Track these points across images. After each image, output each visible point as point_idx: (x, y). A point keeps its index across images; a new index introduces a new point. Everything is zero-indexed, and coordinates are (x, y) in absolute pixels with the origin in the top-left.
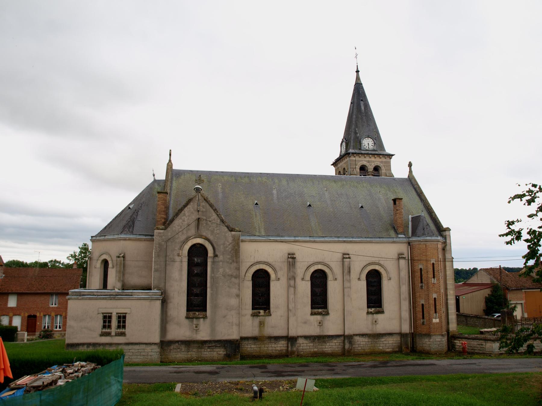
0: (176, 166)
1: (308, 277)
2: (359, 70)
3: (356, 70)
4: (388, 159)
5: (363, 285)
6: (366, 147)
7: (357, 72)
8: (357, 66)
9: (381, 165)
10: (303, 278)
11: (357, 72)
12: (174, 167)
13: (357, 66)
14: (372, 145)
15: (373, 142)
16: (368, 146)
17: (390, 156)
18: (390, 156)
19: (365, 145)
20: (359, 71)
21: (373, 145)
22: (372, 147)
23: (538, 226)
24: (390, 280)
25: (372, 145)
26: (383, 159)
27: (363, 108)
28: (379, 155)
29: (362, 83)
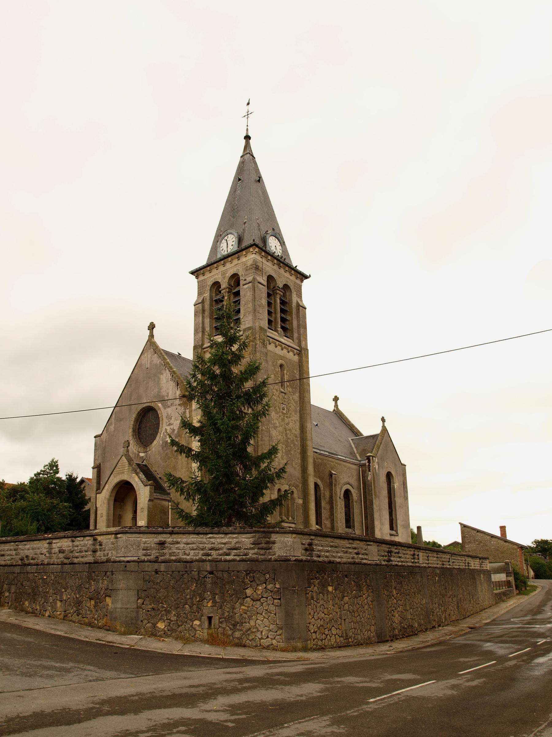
7: (247, 138)
11: (247, 138)
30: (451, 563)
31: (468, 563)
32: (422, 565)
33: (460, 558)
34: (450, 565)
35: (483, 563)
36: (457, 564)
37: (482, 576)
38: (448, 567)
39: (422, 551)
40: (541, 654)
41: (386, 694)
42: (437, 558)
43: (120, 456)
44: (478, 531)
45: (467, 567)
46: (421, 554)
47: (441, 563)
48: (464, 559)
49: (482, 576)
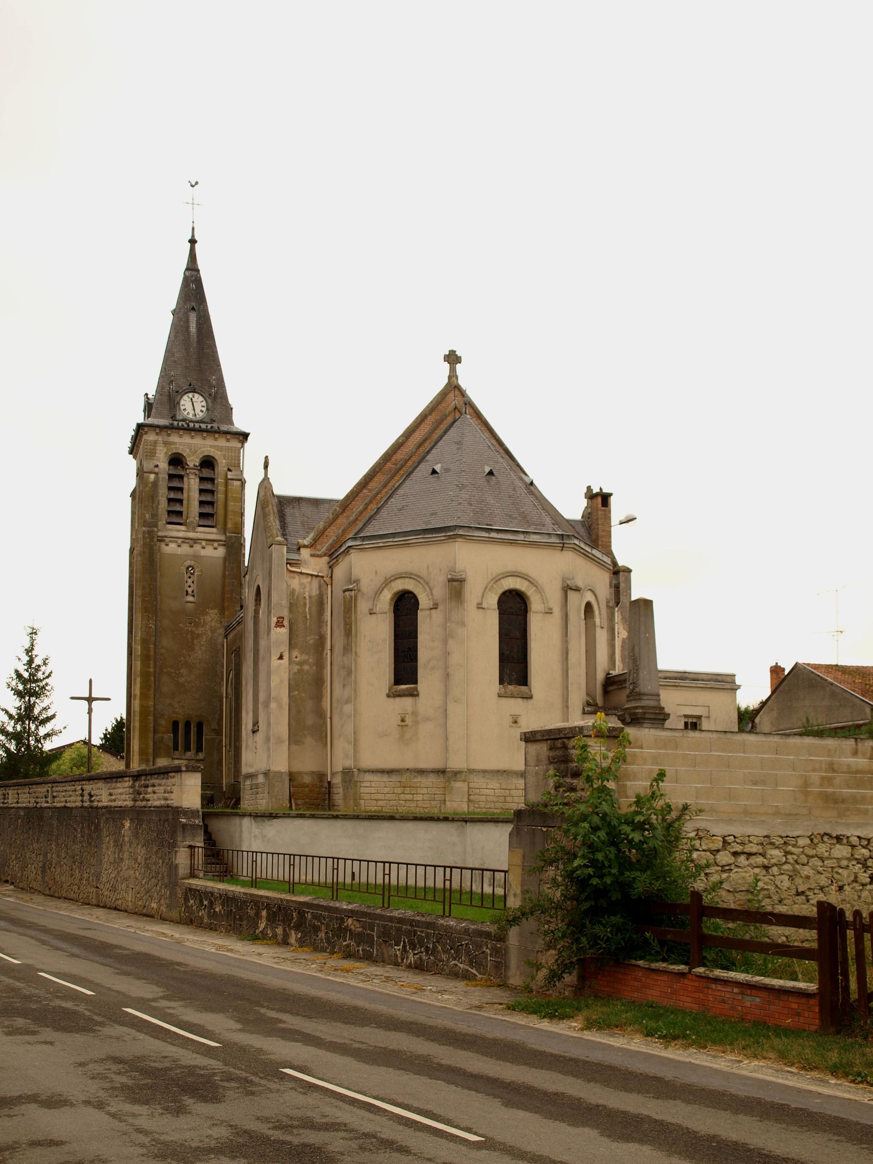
0: (280, 489)
1: (492, 600)
2: (196, 238)
3: (190, 238)
4: (235, 444)
5: (492, 620)
6: (188, 413)
7: (193, 242)
8: (193, 229)
9: (216, 454)
10: (480, 602)
11: (193, 242)
12: (277, 491)
13: (193, 229)
14: (202, 411)
15: (204, 403)
16: (192, 412)
17: (244, 436)
18: (244, 436)
19: (185, 410)
20: (196, 242)
21: (204, 409)
22: (201, 414)
23: (56, 717)
24: (549, 615)
25: (202, 411)
26: (222, 442)
27: (193, 329)
28: (219, 432)
29: (200, 268)
30: (49, 799)
31: (91, 796)
32: (12, 806)
33: (70, 788)
34: (47, 802)
35: (150, 789)
36: (63, 799)
37: (127, 824)
38: (46, 805)
39: (12, 788)
40: (199, 318)
41: (786, 787)
42: (29, 793)
43: (496, 911)
44: (387, 457)
45: (86, 804)
46: (10, 792)
47: (32, 800)
48: (79, 787)
49: (127, 824)
